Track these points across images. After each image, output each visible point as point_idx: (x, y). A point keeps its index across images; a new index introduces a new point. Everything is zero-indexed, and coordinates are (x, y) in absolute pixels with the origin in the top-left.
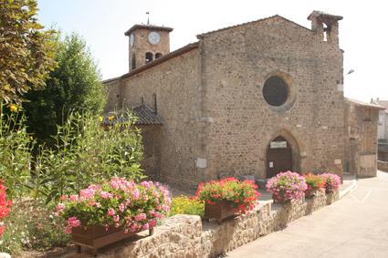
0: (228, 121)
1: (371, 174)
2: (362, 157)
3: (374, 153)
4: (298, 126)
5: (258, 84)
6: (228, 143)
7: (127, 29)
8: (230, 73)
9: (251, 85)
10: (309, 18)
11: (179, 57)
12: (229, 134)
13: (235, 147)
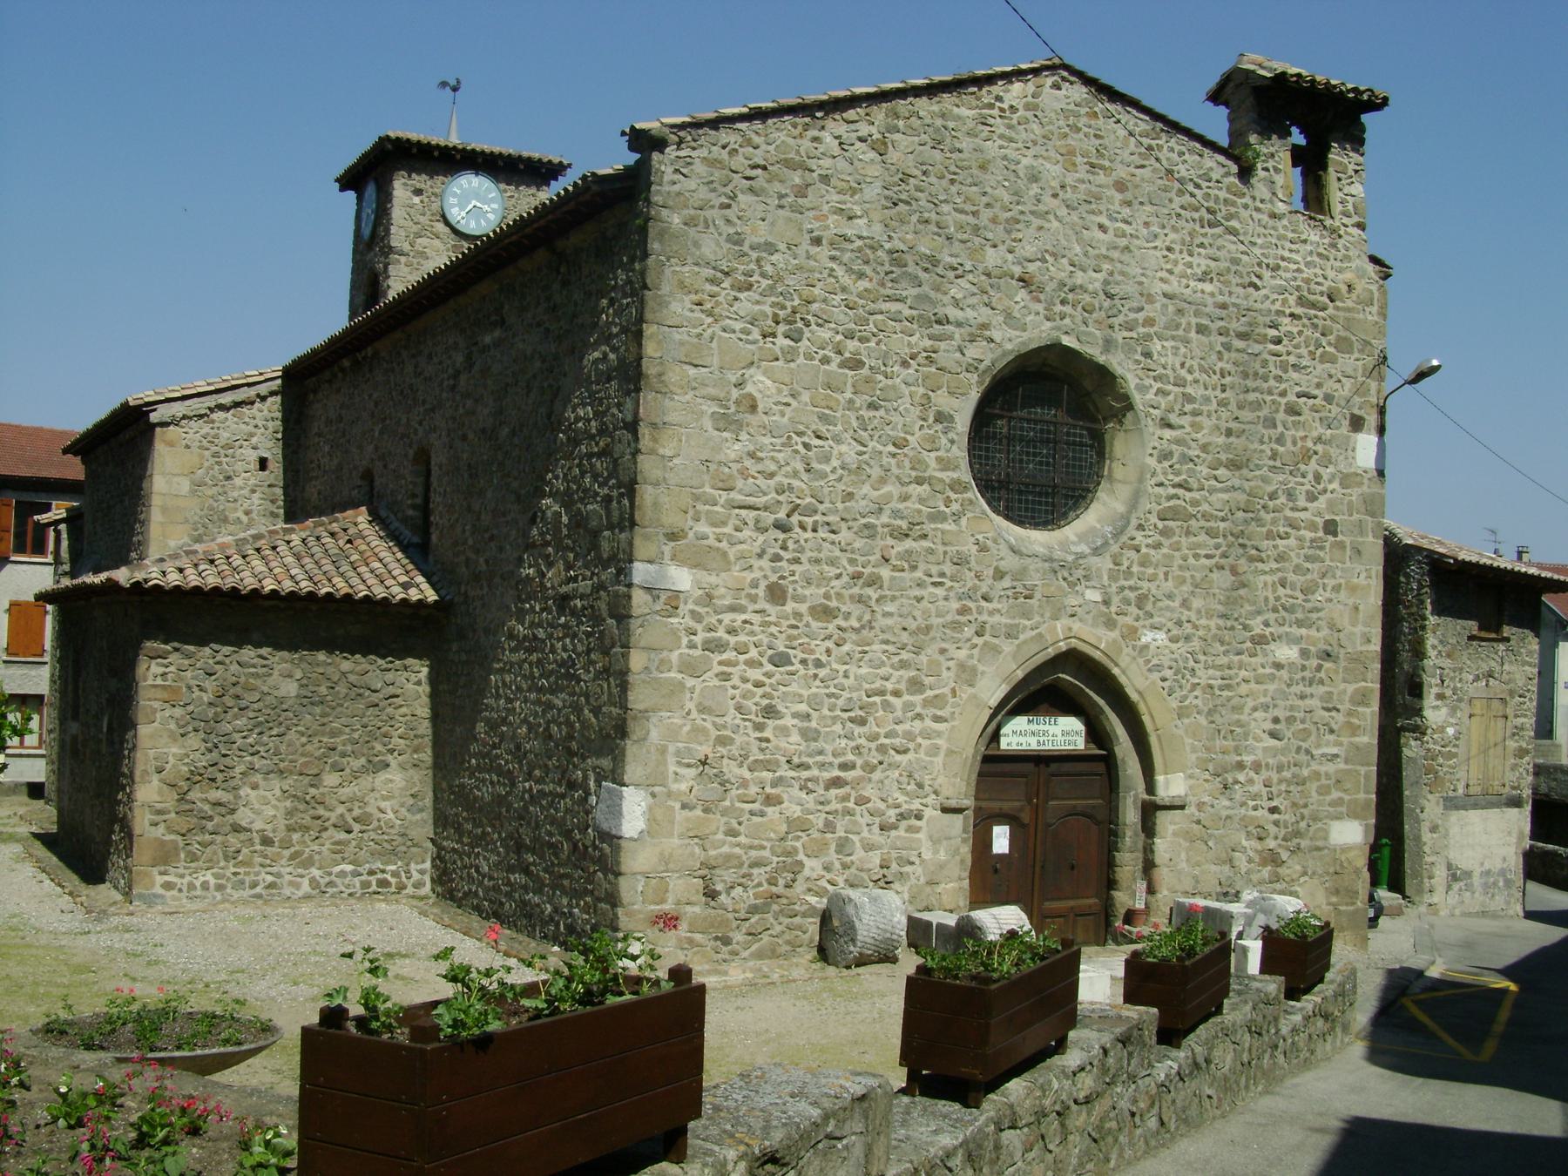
0: (777, 594)
1: (313, 491)
2: (1455, 816)
3: (1516, 802)
4: (1147, 637)
5: (942, 400)
6: (770, 712)
7: (349, 156)
8: (795, 337)
9: (905, 415)
10: (1216, 97)
11: (541, 255)
12: (780, 660)
13: (809, 735)
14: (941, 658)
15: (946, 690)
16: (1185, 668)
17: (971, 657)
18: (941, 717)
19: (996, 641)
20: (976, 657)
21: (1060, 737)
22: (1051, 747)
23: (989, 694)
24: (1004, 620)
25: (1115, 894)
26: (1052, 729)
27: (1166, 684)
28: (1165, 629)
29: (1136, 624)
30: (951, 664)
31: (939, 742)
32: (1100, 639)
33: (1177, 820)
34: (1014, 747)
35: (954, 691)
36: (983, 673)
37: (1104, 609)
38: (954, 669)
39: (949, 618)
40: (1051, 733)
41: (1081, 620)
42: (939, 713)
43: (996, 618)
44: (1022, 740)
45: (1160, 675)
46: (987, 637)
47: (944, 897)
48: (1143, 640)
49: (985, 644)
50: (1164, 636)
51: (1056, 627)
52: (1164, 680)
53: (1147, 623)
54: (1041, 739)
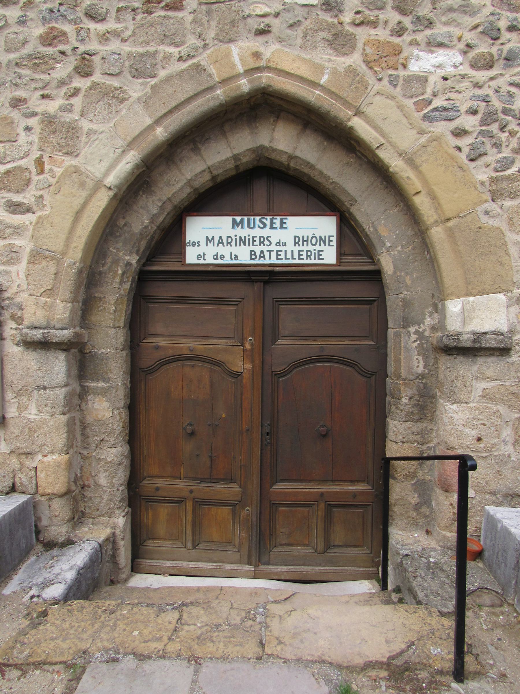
14: (15, 114)
15: (28, 163)
16: (505, 112)
17: (69, 108)
18: (19, 205)
19: (115, 83)
20: (77, 108)
21: (290, 247)
22: (274, 260)
23: (104, 165)
24: (127, 48)
25: (42, 545)
26: (276, 235)
27: (465, 142)
28: (461, 46)
29: (396, 40)
30: (33, 122)
31: (18, 242)
32: (320, 69)
33: (490, 373)
34: (210, 260)
35: (40, 163)
36: (90, 133)
37: (328, 18)
38: (37, 129)
39: (27, 50)
40: (274, 240)
41: (281, 40)
42: (17, 198)
43: (115, 45)
44: (223, 250)
45: (453, 125)
46: (97, 77)
47: (41, 475)
48: (414, 67)
49: (94, 86)
50: (459, 59)
51: (229, 54)
52: (460, 133)
53: (420, 37)
54: (258, 250)
